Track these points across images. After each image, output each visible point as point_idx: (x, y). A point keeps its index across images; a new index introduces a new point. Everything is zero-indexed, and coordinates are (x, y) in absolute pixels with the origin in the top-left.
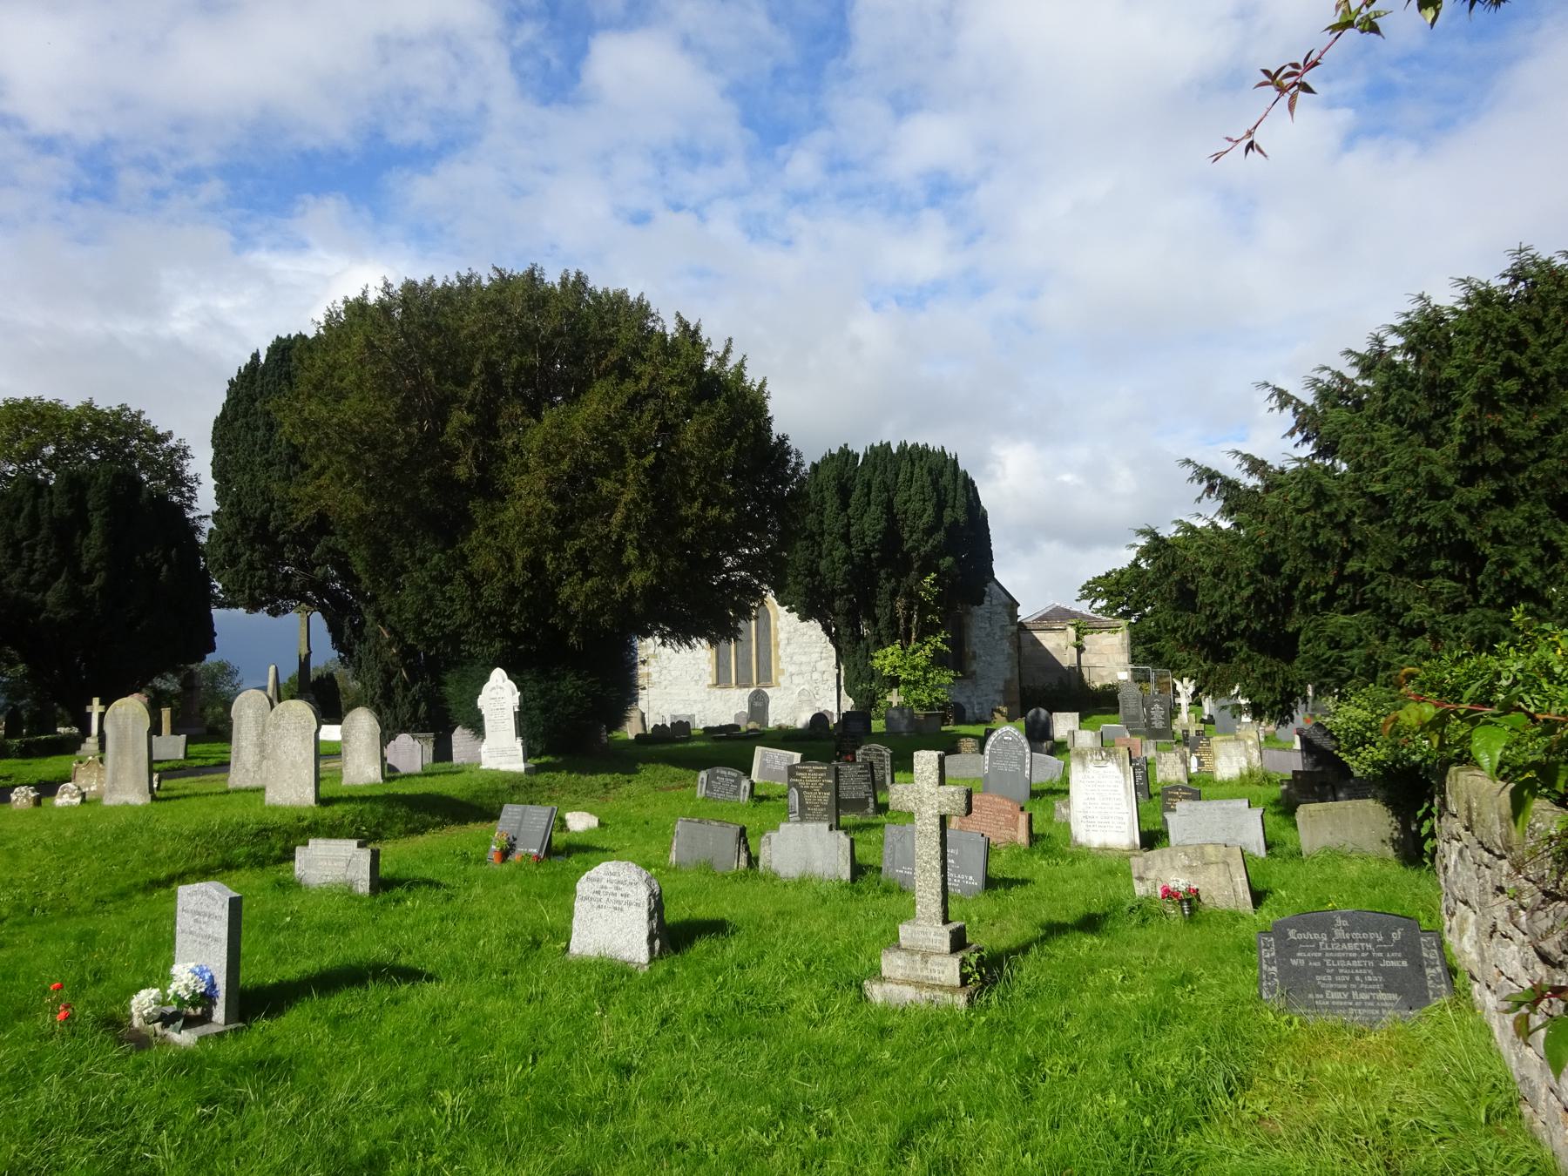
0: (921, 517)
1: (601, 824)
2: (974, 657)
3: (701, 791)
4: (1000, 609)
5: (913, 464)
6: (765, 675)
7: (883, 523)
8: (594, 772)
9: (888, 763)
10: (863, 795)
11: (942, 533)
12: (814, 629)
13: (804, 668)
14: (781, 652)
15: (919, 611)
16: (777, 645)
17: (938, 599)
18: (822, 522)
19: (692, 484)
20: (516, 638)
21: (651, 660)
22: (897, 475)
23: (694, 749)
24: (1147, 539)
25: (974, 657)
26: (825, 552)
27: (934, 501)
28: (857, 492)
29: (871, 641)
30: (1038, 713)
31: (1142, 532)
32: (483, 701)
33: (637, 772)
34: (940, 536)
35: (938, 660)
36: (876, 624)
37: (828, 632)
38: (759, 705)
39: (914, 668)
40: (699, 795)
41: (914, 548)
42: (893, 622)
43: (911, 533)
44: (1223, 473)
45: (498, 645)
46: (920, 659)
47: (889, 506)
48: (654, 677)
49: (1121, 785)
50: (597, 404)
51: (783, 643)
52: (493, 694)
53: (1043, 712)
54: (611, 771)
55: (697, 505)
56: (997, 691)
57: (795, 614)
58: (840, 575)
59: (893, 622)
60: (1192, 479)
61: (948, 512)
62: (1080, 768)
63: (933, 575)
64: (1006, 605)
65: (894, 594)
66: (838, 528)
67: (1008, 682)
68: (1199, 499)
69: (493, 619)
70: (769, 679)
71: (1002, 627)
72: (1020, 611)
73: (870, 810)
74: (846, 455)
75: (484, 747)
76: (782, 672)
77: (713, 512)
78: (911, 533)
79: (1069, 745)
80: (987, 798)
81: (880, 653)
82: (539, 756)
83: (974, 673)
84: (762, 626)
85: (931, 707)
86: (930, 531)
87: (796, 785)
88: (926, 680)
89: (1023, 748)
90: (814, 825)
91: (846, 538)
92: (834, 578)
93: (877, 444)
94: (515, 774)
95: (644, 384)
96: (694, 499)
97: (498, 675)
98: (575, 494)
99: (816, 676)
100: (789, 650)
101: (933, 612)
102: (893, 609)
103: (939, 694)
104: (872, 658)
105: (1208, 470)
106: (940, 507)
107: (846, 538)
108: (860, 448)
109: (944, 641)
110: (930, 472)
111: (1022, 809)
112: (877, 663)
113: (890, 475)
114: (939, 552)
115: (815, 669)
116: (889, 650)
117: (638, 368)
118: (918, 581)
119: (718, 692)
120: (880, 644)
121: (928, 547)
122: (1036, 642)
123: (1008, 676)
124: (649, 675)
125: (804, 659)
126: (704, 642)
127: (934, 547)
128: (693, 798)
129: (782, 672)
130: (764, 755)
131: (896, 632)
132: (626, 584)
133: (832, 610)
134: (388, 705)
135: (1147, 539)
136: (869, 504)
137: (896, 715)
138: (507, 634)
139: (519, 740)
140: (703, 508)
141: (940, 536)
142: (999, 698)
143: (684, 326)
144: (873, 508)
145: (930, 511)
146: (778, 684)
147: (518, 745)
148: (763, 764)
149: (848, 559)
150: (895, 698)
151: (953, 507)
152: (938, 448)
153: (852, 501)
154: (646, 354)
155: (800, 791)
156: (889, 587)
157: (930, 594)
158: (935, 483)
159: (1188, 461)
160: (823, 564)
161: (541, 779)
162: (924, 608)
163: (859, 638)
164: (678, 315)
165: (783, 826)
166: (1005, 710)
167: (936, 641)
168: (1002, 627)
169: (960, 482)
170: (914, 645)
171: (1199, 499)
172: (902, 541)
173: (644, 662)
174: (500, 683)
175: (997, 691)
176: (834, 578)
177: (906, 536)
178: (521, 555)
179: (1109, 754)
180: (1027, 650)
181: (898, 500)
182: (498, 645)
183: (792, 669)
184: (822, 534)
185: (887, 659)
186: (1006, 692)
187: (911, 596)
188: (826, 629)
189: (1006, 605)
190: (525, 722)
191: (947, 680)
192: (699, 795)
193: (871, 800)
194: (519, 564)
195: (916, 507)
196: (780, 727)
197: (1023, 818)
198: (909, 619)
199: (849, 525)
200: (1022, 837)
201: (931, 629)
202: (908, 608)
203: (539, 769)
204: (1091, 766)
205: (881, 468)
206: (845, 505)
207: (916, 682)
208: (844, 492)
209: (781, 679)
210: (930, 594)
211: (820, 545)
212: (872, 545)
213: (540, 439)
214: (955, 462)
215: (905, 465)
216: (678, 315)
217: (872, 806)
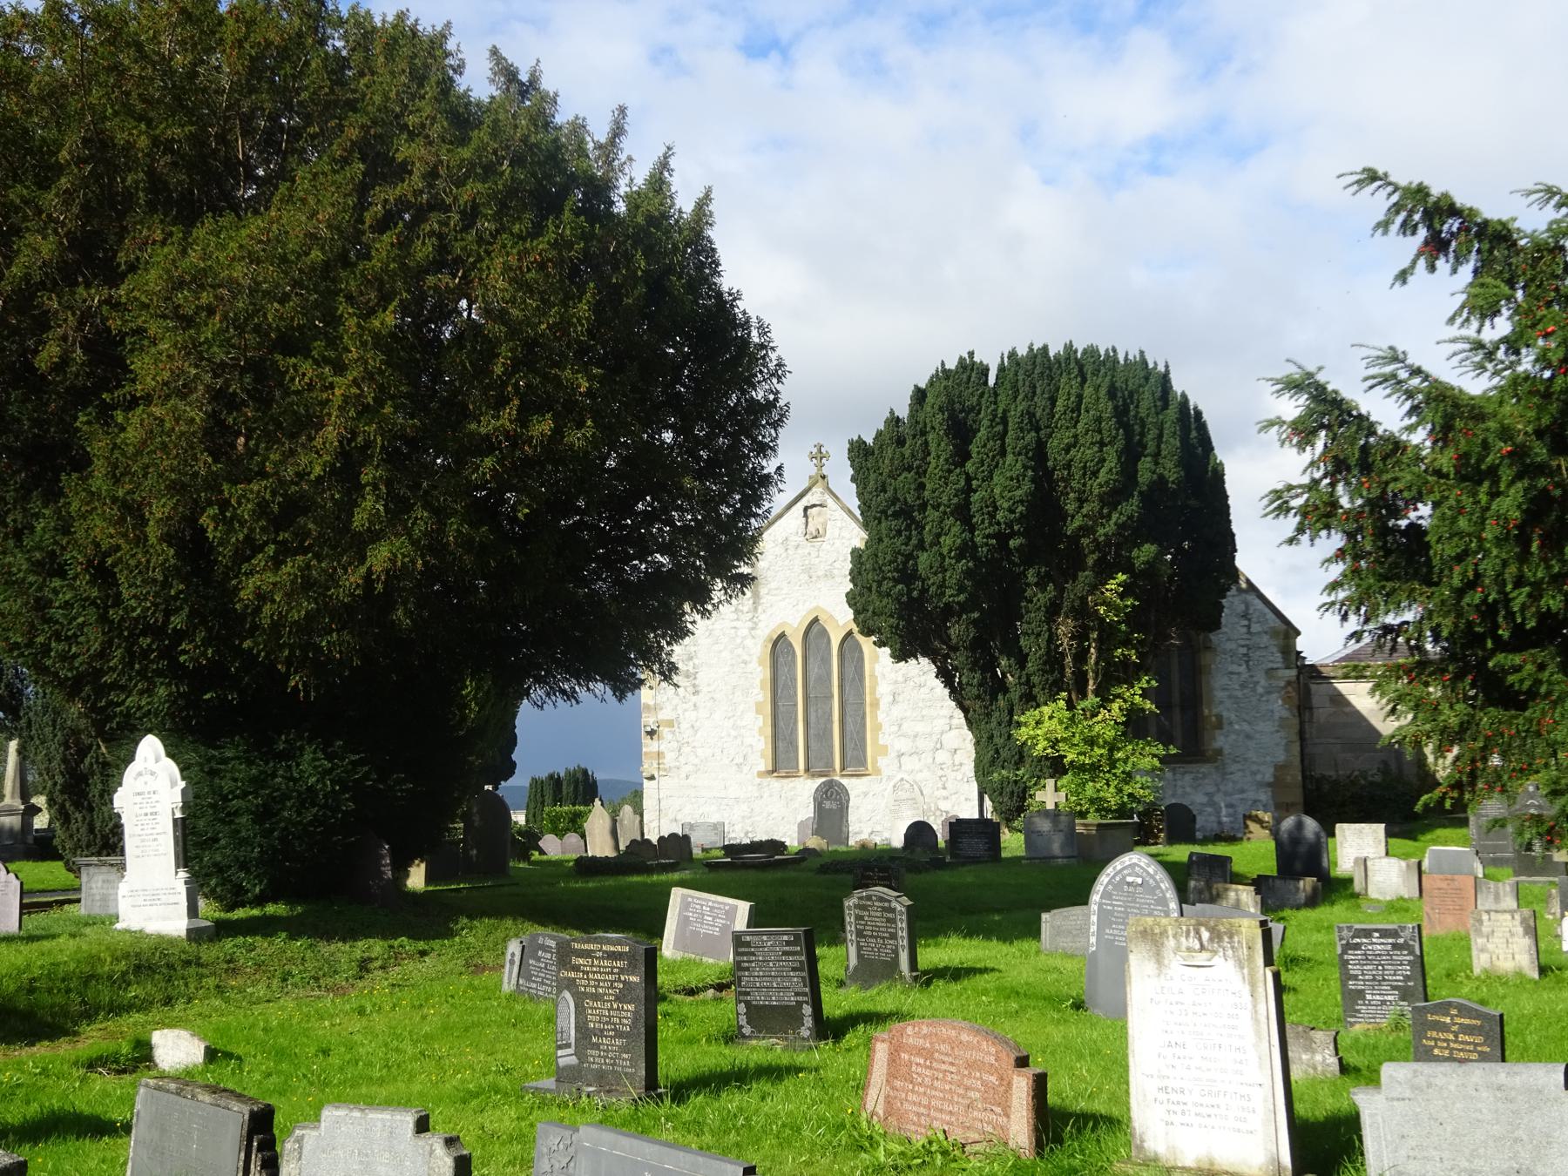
0: (1095, 474)
1: (211, 1055)
2: (1219, 725)
3: (509, 980)
4: (1265, 640)
5: (1084, 380)
6: (856, 759)
7: (1027, 486)
8: (351, 935)
9: (902, 925)
10: (790, 999)
11: (1135, 501)
12: (922, 670)
13: (922, 744)
14: (881, 716)
15: (1100, 640)
16: (875, 704)
17: (1134, 619)
18: (922, 486)
19: (498, 370)
20: (198, 678)
21: (664, 731)
22: (1053, 401)
23: (631, 886)
24: (1303, 399)
25: (1219, 725)
26: (928, 539)
27: (1120, 444)
28: (982, 433)
29: (1015, 695)
30: (1300, 826)
31: (1293, 386)
32: (123, 800)
33: (450, 934)
34: (1131, 507)
35: (1135, 725)
36: (1022, 666)
37: (948, 683)
38: (831, 807)
39: (1091, 742)
40: (508, 986)
41: (1085, 530)
42: (1053, 660)
43: (1081, 501)
44: (1461, 199)
45: (162, 692)
46: (1107, 722)
47: (1039, 453)
48: (669, 759)
49: (1246, 1015)
50: (306, 209)
51: (885, 701)
52: (139, 785)
53: (1311, 825)
54: (388, 933)
55: (510, 411)
56: (1261, 785)
57: (887, 650)
58: (953, 578)
59: (1053, 660)
60: (1384, 225)
61: (1145, 464)
62: (1150, 967)
63: (1121, 577)
64: (1274, 633)
65: (1053, 611)
66: (948, 496)
67: (1280, 769)
68: (1403, 277)
69: (145, 642)
70: (862, 762)
71: (1270, 672)
72: (1301, 644)
73: (805, 1032)
74: (970, 370)
75: (123, 888)
76: (884, 750)
77: (543, 426)
78: (1081, 501)
79: (1358, 886)
80: (945, 1032)
81: (1030, 716)
82: (260, 901)
83: (1219, 752)
84: (850, 671)
85: (1122, 811)
86: (1113, 498)
87: (571, 985)
88: (1113, 764)
89: (1163, 902)
90: (386, 1116)
91: (962, 512)
92: (942, 585)
93: (1022, 351)
94: (172, 941)
95: (416, 181)
96: (501, 402)
97: (150, 748)
98: (253, 392)
99: (942, 756)
100: (896, 712)
101: (1126, 643)
102: (1052, 637)
103: (1134, 788)
104: (1019, 725)
105: (1421, 192)
106: (1131, 455)
107: (962, 512)
108: (991, 358)
109: (1145, 694)
110: (1112, 393)
111: (1022, 1062)
112: (1022, 734)
113: (1041, 401)
114: (1133, 533)
115: (939, 746)
116: (1047, 710)
117: (404, 150)
118: (1094, 588)
119: (775, 784)
120: (1030, 700)
121: (1110, 528)
122: (1340, 700)
123: (1281, 757)
124: (659, 755)
125: (920, 728)
126: (599, 687)
127: (1121, 527)
128: (493, 991)
129: (884, 750)
130: (686, 905)
131: (1060, 679)
132: (363, 570)
133: (946, 640)
134: (78, 805)
135: (1303, 399)
136: (1003, 453)
137: (1045, 825)
138: (176, 672)
139: (183, 874)
140: (523, 420)
141: (1131, 507)
142: (1264, 796)
143: (508, 74)
144: (1010, 458)
145: (1112, 462)
146: (878, 772)
147: (177, 883)
148: (684, 922)
149: (966, 550)
150: (1049, 795)
151: (1157, 455)
152: (1134, 355)
153: (973, 448)
154: (412, 120)
155: (579, 998)
156: (1042, 598)
157: (1117, 610)
158: (1121, 413)
159: (1372, 176)
160: (924, 559)
161: (209, 952)
162: (1109, 638)
163: (1000, 686)
164: (494, 52)
165: (328, 1114)
166: (1267, 817)
167: (1135, 694)
168: (1270, 672)
169: (1172, 413)
170: (1092, 700)
171: (1403, 277)
172: (1063, 516)
173: (651, 733)
174: (151, 765)
175: (1261, 785)
176: (942, 585)
177: (1071, 507)
178: (159, 509)
179: (1216, 936)
180: (1322, 712)
181: (1054, 445)
182: (162, 692)
183: (902, 745)
184: (923, 507)
185: (1042, 726)
186: (1277, 785)
187: (1082, 612)
188: (945, 675)
189: (1274, 633)
190: (194, 842)
191: (1147, 762)
192: (508, 986)
193: (807, 1010)
194: (153, 532)
195: (1088, 461)
196: (863, 846)
197: (1021, 1085)
198: (1081, 656)
199: (969, 490)
200: (1020, 1130)
201: (1124, 673)
202: (1080, 636)
203: (222, 929)
204: (1174, 963)
205: (1024, 390)
206: (962, 456)
207: (1094, 768)
208: (961, 432)
209: (882, 762)
210: (1117, 610)
211: (921, 528)
212: (1009, 525)
213: (187, 281)
214: (1165, 378)
215: (1068, 386)
216: (494, 52)
217: (808, 1022)
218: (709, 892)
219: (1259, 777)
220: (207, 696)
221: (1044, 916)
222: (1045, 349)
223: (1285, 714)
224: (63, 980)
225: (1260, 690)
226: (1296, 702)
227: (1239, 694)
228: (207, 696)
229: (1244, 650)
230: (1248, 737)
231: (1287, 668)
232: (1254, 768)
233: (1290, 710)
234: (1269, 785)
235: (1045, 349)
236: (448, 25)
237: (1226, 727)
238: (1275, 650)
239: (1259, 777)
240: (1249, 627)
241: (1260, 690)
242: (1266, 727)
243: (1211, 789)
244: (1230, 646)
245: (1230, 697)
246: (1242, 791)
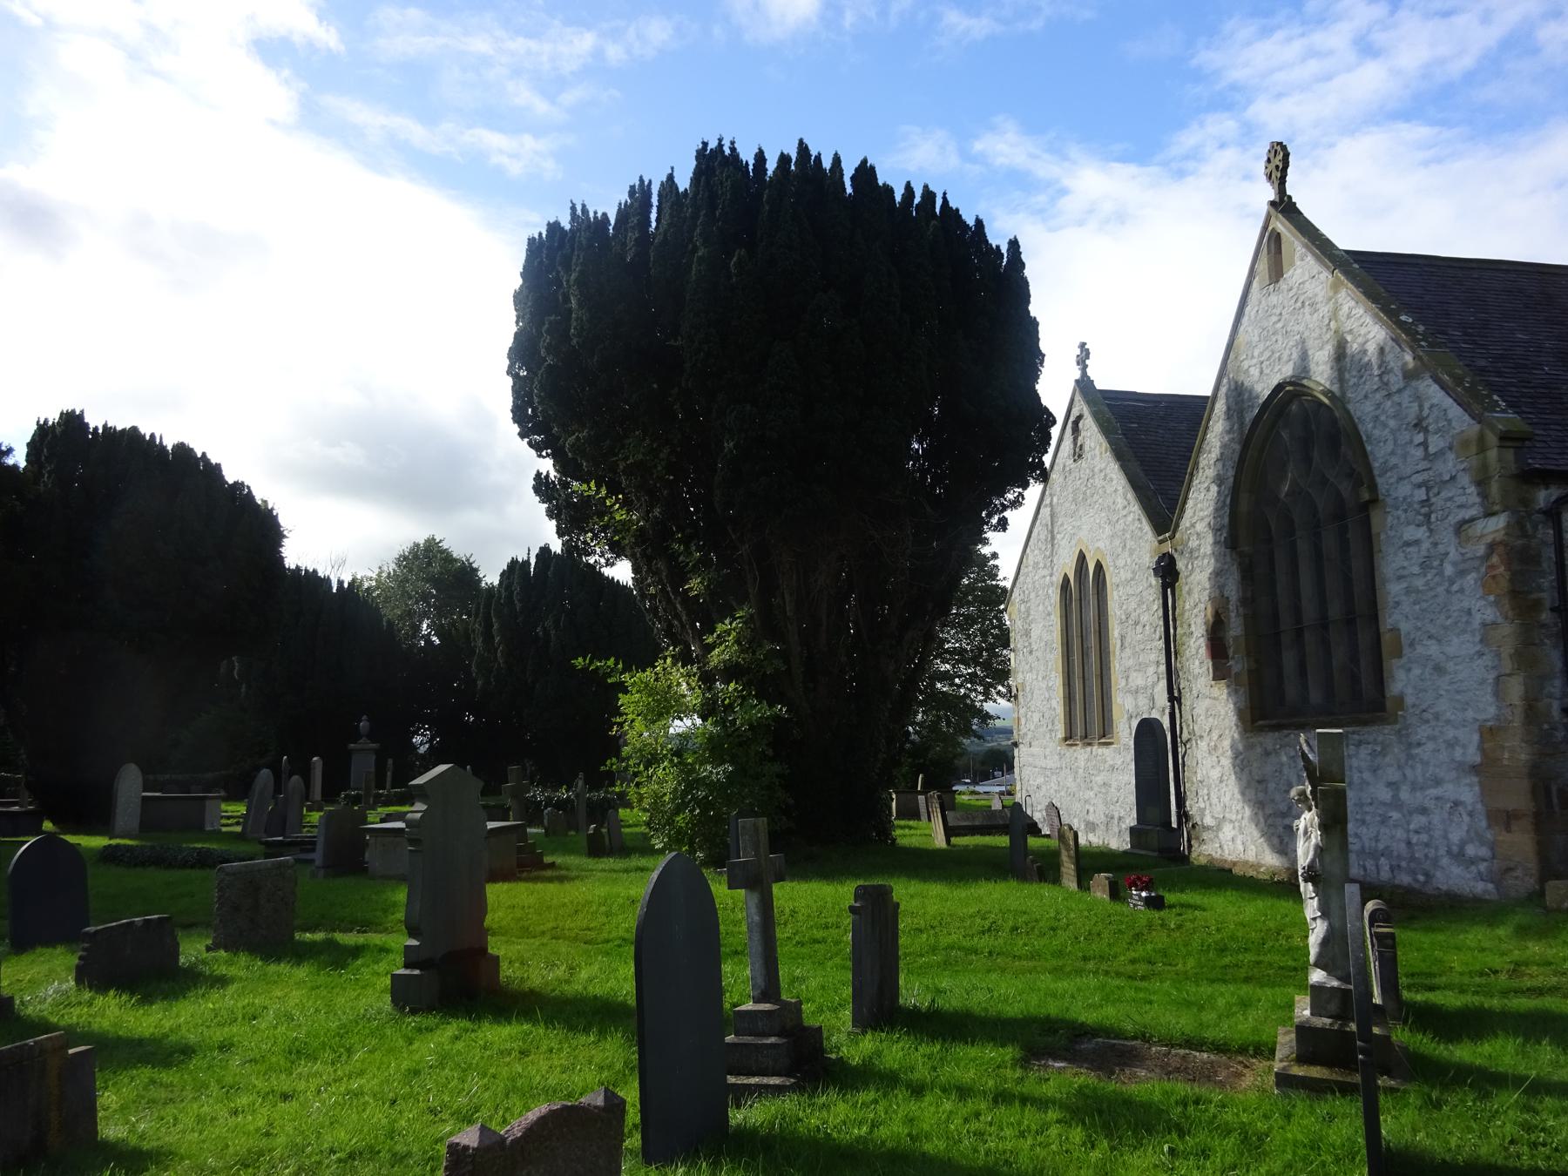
119: (1081, 754)
123: (1489, 710)
218: (982, 834)
219: (1458, 753)
220: (622, 572)
221: (496, 583)
222: (46, 421)
223: (1490, 614)
224: (411, 571)
225: (1449, 570)
226: (1504, 584)
227: (1419, 583)
228: (622, 572)
229: (1421, 494)
230: (1439, 669)
231: (1489, 514)
232: (1451, 733)
233: (1496, 603)
234: (1475, 769)
235: (46, 421)
236: (801, 142)
237: (1406, 650)
238: (1465, 480)
239: (1458, 753)
240: (1425, 444)
241: (1449, 570)
242: (1461, 645)
243: (1393, 774)
244: (1404, 490)
245: (1408, 591)
246: (1438, 782)
